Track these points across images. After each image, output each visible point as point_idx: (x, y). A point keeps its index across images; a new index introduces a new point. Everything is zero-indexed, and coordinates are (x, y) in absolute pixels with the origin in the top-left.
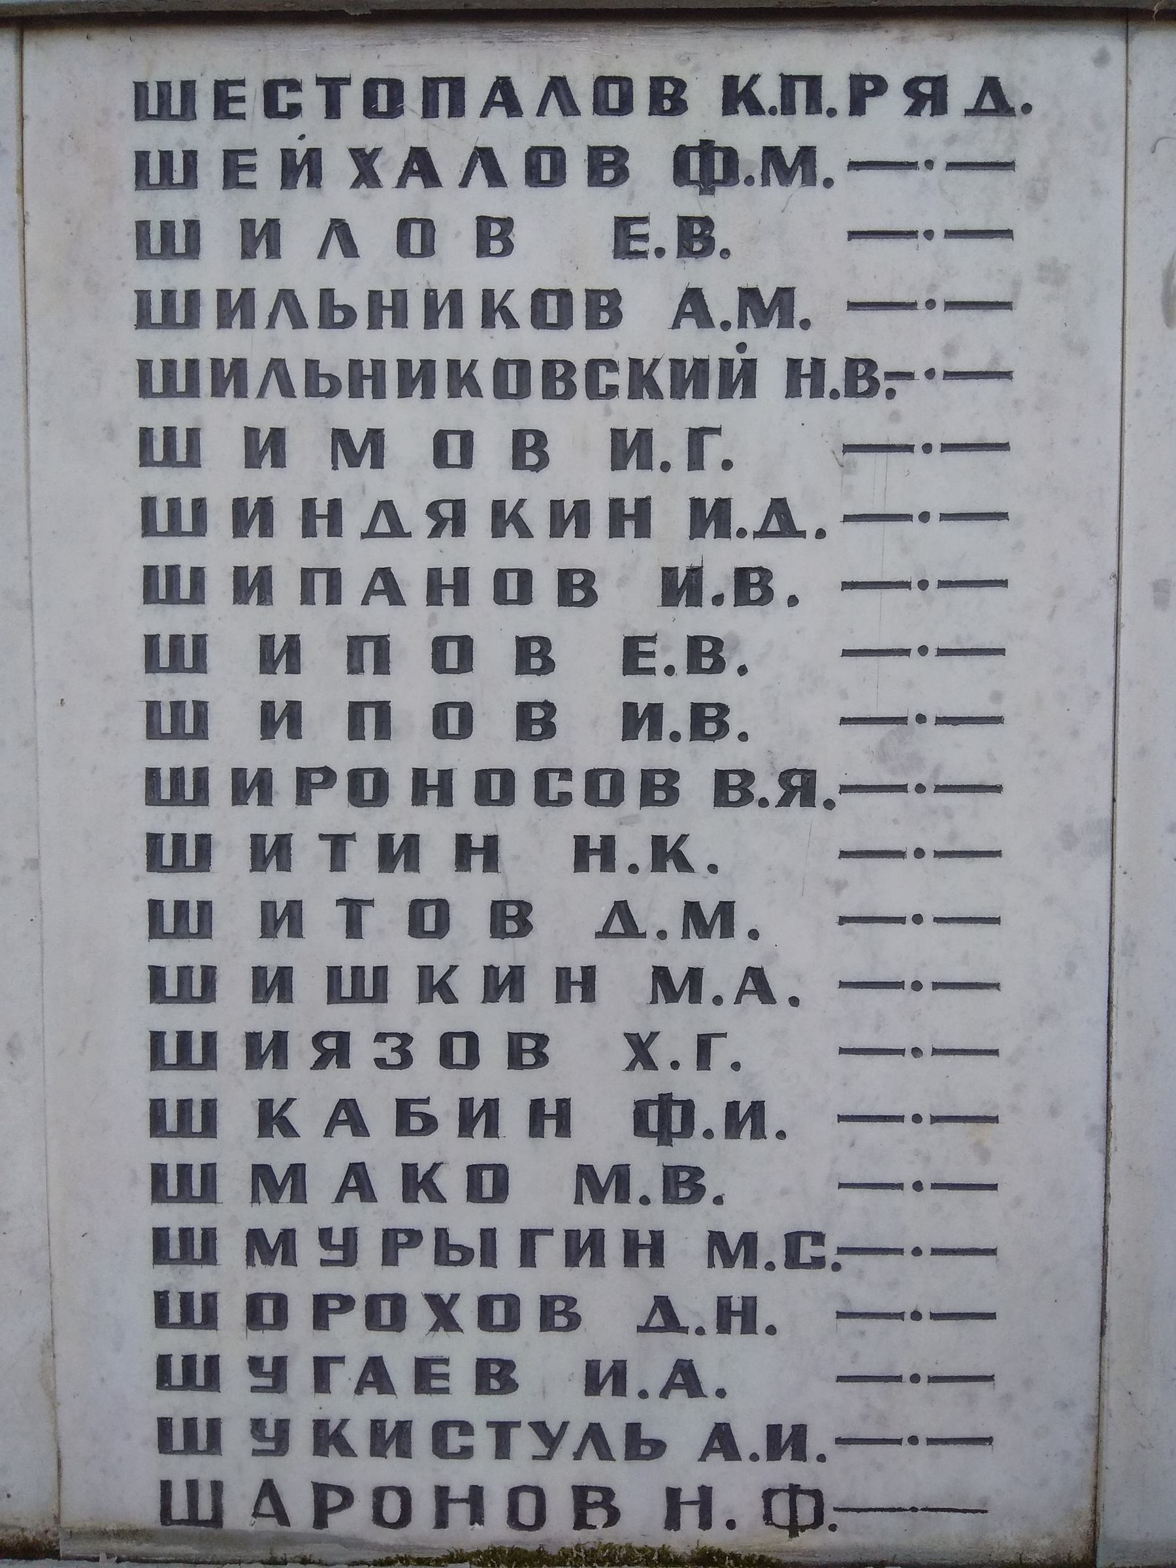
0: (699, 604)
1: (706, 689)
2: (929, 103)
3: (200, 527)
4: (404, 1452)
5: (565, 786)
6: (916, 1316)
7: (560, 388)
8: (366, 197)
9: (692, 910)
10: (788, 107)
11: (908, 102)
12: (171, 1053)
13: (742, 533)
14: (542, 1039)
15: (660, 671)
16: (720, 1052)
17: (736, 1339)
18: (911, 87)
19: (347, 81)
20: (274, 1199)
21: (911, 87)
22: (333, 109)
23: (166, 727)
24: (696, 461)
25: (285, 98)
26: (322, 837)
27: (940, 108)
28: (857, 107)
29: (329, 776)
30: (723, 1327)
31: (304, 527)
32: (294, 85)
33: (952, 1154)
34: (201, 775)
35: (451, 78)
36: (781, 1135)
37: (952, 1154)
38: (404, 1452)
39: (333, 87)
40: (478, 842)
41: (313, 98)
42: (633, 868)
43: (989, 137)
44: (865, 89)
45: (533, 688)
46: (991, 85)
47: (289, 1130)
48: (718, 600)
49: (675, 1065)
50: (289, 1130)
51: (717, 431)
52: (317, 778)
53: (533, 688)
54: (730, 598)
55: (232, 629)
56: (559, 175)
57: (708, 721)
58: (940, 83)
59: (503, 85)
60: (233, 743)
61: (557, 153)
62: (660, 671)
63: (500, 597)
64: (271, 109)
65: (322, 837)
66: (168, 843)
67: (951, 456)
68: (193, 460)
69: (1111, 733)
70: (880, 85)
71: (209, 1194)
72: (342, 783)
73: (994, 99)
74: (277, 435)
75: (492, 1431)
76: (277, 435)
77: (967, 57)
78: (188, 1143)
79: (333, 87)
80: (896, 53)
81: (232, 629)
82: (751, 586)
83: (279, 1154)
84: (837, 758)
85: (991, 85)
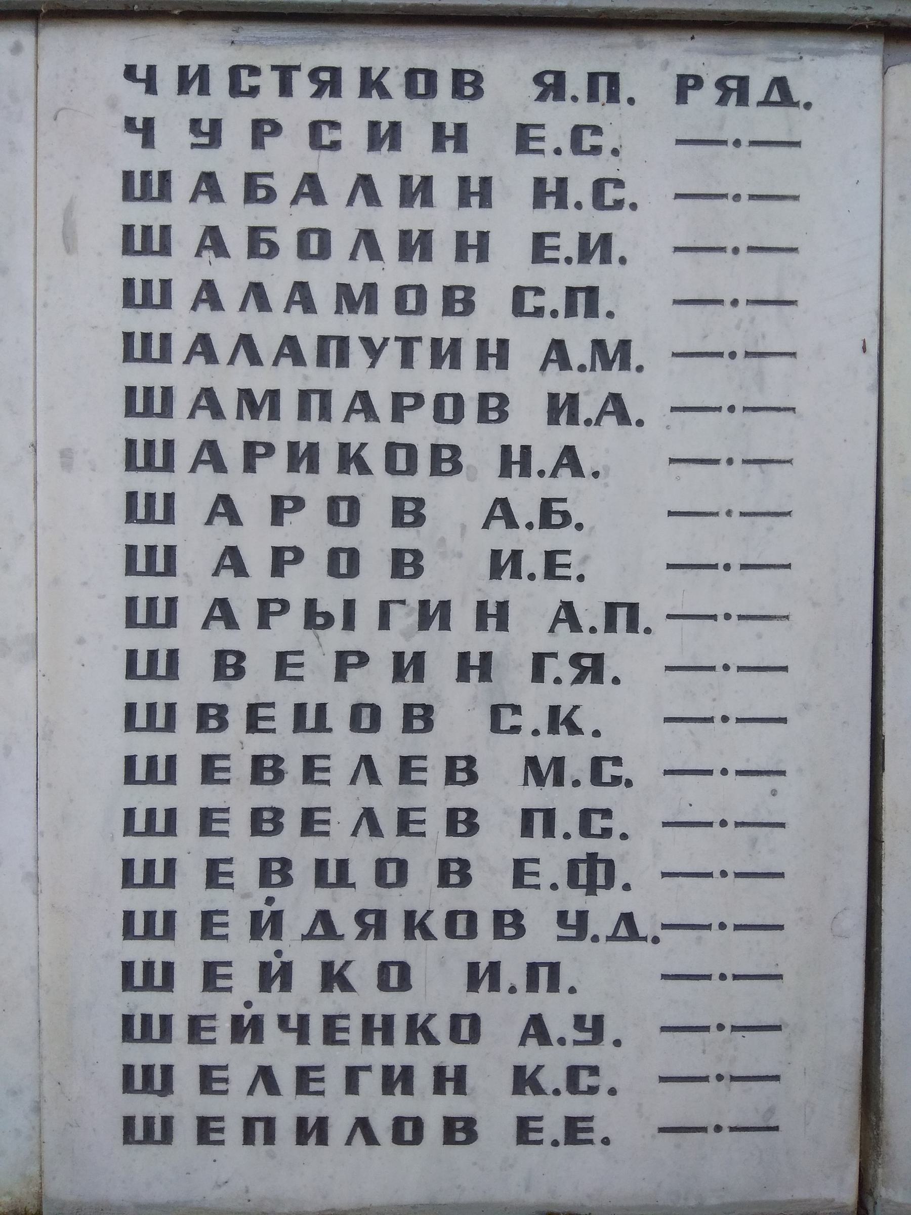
0: (529, 475)
3: (170, 725)
9: (599, 345)
12: (141, 772)
13: (595, 939)
15: (562, 260)
18: (721, 83)
19: (298, 68)
21: (721, 83)
22: (286, 89)
23: (138, 246)
25: (246, 82)
26: (353, 885)
27: (743, 100)
29: (270, 449)
32: (254, 71)
34: (166, 1020)
39: (285, 73)
41: (269, 82)
42: (575, 99)
43: (773, 122)
45: (406, 538)
46: (780, 83)
48: (530, 526)
52: (260, 450)
53: (406, 538)
55: (194, 490)
58: (743, 81)
60: (186, 998)
62: (562, 260)
64: (235, 90)
65: (353, 885)
66: (141, 501)
68: (169, 518)
70: (699, 82)
71: (167, 1087)
73: (782, 92)
75: (276, 74)
78: (146, 312)
79: (285, 73)
81: (194, 490)
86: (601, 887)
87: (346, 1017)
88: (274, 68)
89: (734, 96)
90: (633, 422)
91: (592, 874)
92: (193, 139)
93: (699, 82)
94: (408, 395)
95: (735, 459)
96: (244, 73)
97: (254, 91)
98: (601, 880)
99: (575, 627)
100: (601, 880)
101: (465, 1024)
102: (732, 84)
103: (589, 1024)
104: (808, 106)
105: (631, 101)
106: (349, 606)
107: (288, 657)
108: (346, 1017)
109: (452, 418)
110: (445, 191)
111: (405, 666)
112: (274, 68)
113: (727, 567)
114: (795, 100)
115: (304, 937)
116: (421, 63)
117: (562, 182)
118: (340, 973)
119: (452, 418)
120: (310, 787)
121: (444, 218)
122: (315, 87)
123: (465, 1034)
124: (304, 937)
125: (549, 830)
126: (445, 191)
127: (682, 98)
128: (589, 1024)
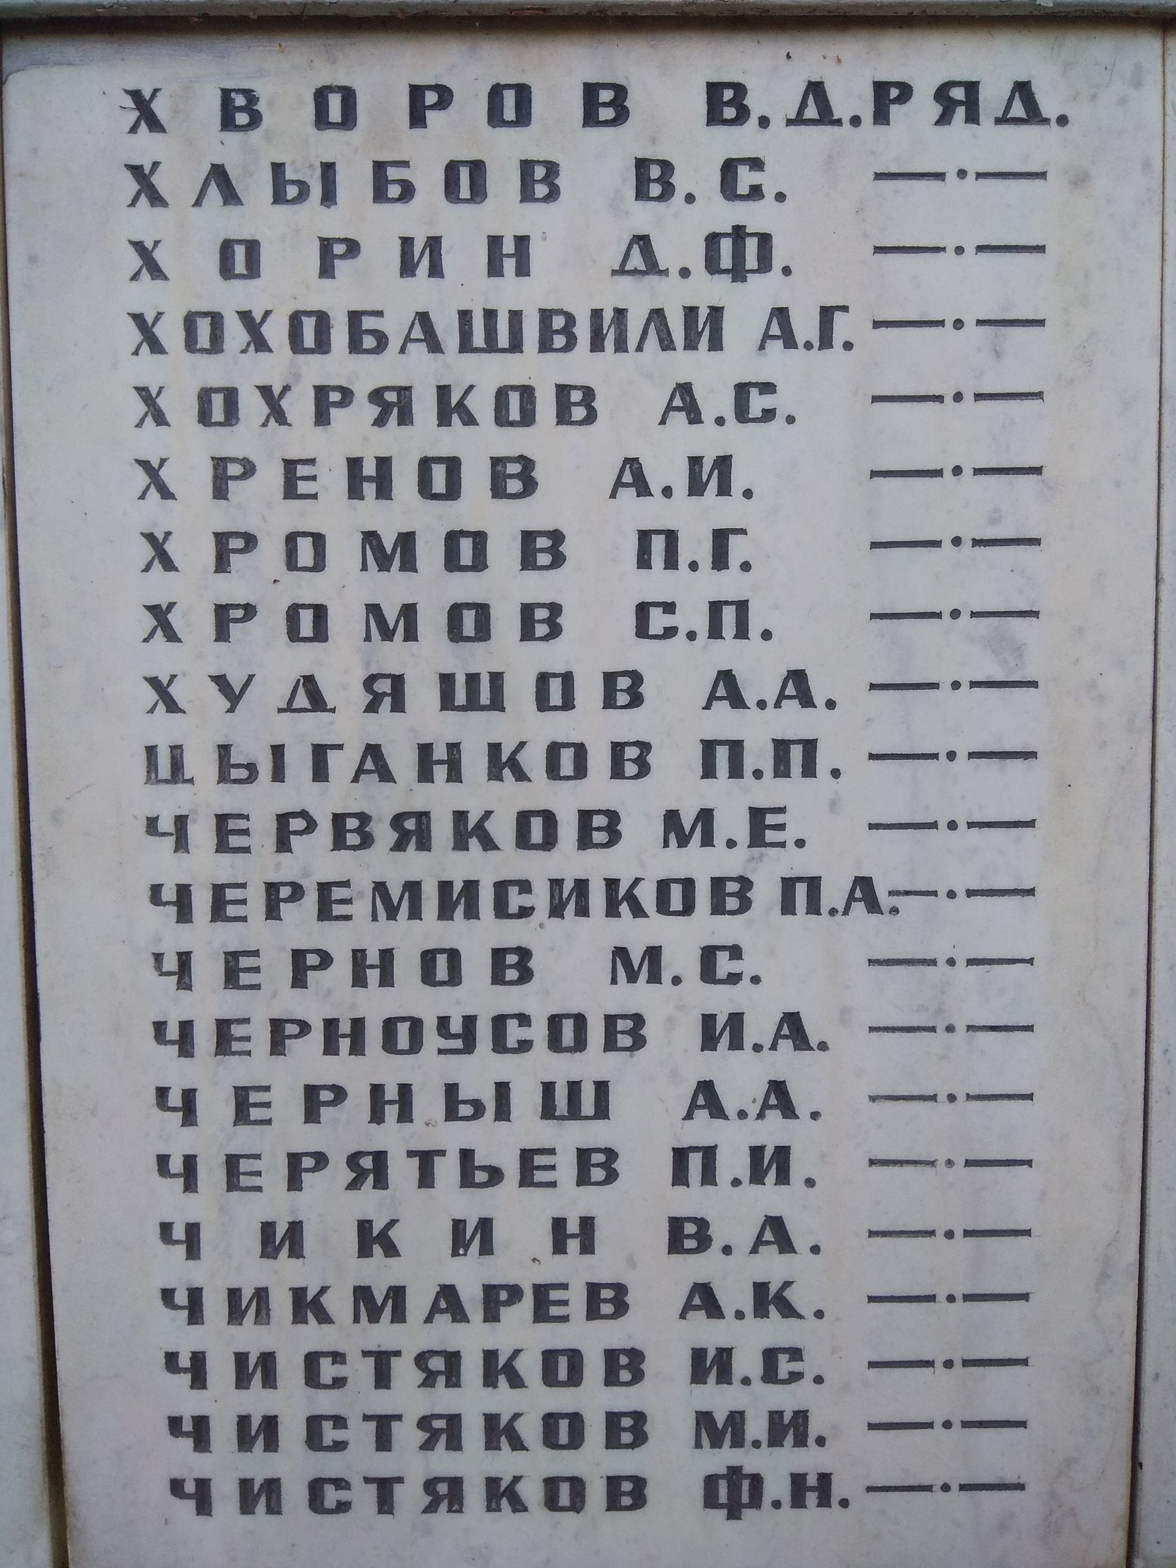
1: (786, 1399)
5: (526, 900)
7: (541, 190)
8: (271, 104)
10: (757, 1176)
11: (428, 1499)
13: (757, 1048)
14: (557, 537)
16: (738, 549)
17: (812, 1511)
24: (720, 560)
27: (973, 117)
28: (881, 116)
30: (798, 1501)
31: (218, 1044)
35: (380, 1416)
44: (888, 97)
46: (1023, 89)
51: (743, 532)
54: (768, 771)
56: (578, 1503)
57: (773, 1164)
58: (972, 88)
61: (549, 819)
67: (928, 1292)
69: (1157, 843)
72: (311, 898)
77: (993, 62)
80: (928, 60)
82: (795, 757)
86: (752, 271)
87: (564, 1286)
89: (960, 112)
90: (801, 344)
91: (738, 254)
93: (906, 91)
94: (233, 460)
98: (751, 262)
99: (695, 417)
100: (751, 262)
101: (218, 401)
102: (958, 94)
104: (1063, 120)
106: (502, 1089)
108: (564, 1286)
109: (339, 120)
110: (504, 551)
111: (455, 897)
113: (958, 324)
114: (1044, 116)
116: (342, 78)
118: (480, 826)
119: (339, 120)
120: (233, 993)
121: (505, 586)
122: (428, 1499)
123: (218, 414)
125: (671, 562)
126: (504, 551)
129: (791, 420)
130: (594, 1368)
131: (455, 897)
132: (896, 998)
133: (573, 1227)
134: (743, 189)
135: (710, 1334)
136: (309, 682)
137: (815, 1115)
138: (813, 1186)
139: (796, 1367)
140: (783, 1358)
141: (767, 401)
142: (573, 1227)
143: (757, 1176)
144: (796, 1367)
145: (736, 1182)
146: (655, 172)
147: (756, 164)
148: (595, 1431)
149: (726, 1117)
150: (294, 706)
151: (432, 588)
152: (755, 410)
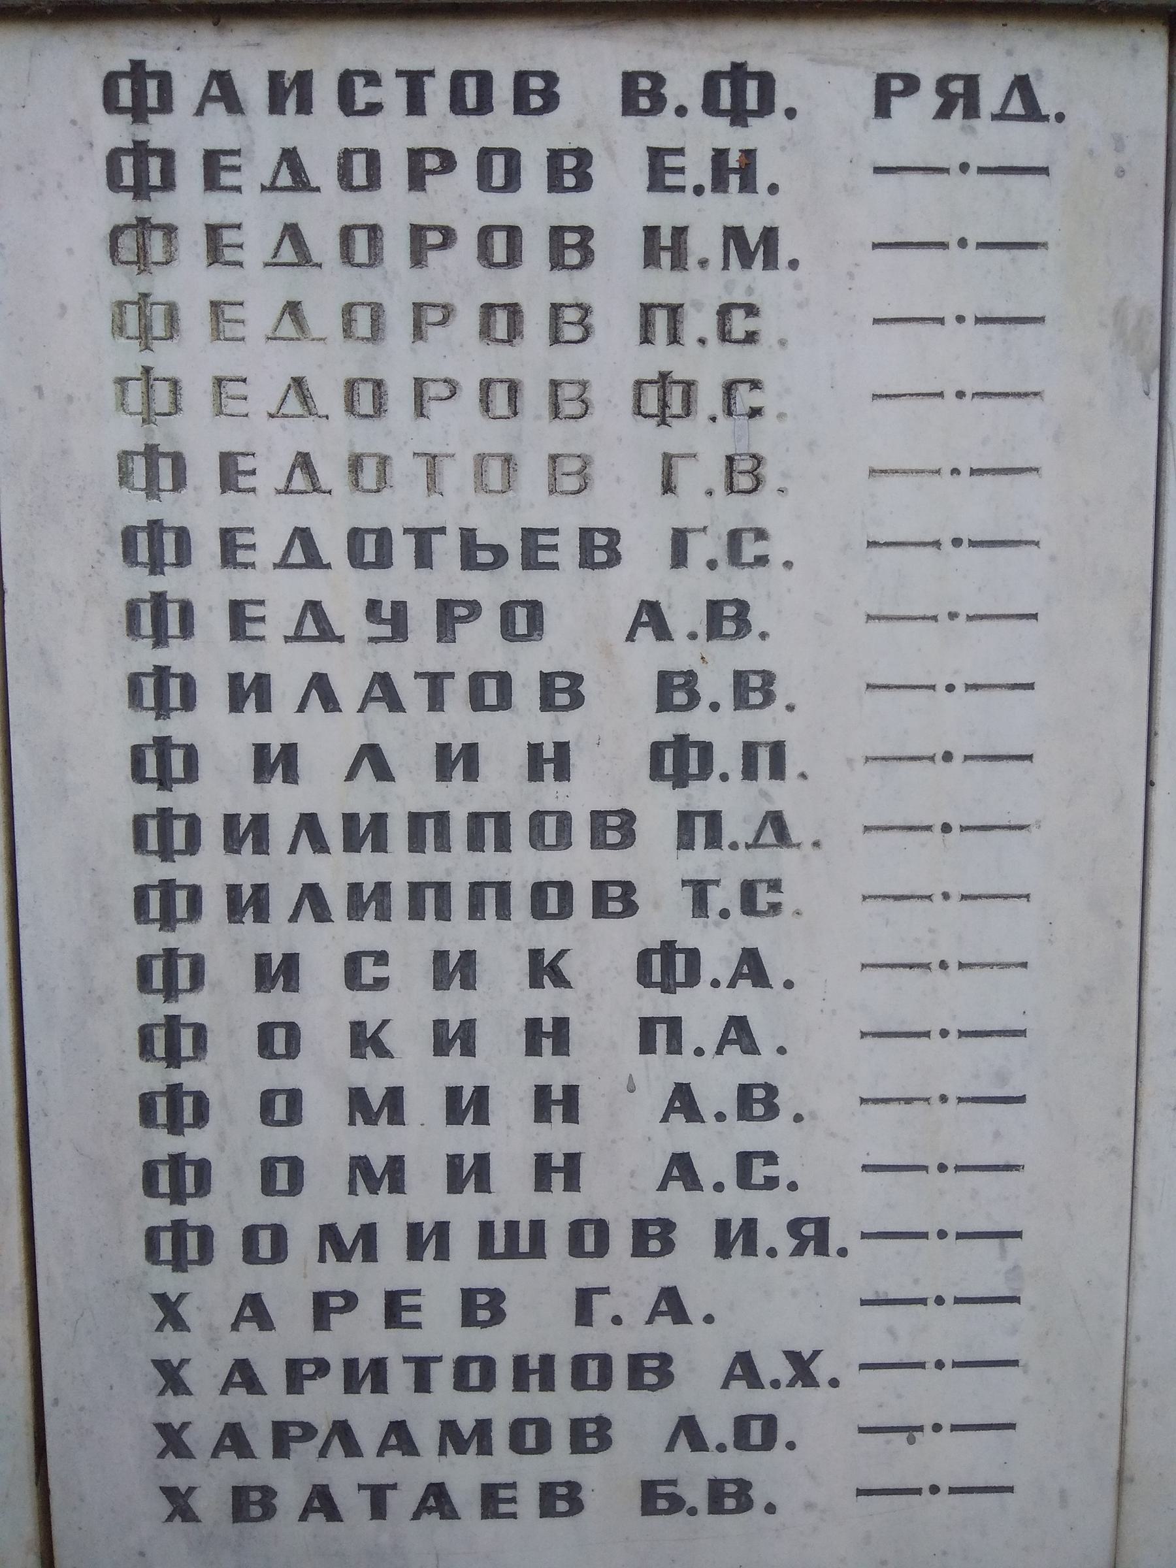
2: (812, 1243)
4: (380, 846)
6: (940, 1300)
10: (719, 184)
20: (373, 1189)
25: (363, 95)
26: (361, 1487)
27: (971, 111)
32: (372, 79)
33: (982, 1269)
36: (789, 984)
37: (982, 1269)
38: (380, 846)
39: (415, 81)
40: (558, 1161)
43: (1022, 142)
46: (1022, 84)
47: (383, 1052)
49: (703, 263)
50: (383, 1052)
58: (971, 82)
59: (222, 78)
63: (602, 1227)
65: (361, 1487)
69: (1139, 1150)
70: (911, 84)
74: (468, 957)
75: (402, 83)
76: (468, 957)
77: (991, 54)
79: (415, 81)
83: (375, 1076)
84: (852, 1205)
85: (1022, 84)
88: (399, 74)
92: (678, 1491)
95: (955, 755)
96: (359, 82)
97: (373, 109)
102: (957, 87)
103: (386, 613)
104: (1060, 117)
105: (791, 113)
107: (331, 1299)
111: (465, 1174)
112: (399, 74)
115: (276, 566)
117: (680, 233)
124: (276, 566)
127: (882, 109)
128: (386, 613)
129: (793, 1186)
130: (534, 172)
131: (465, 1174)
132: (877, 1335)
133: (557, 1112)
134: (738, 334)
135: (666, 211)
136: (313, 607)
137: (788, 564)
138: (790, 568)
139: (771, 1171)
140: (757, 1163)
141: (760, 548)
142: (557, 1112)
143: (719, 184)
144: (771, 1171)
145: (715, 983)
146: (645, 84)
147: (755, 384)
148: (536, 247)
149: (763, 1387)
150: (290, 561)
151: (534, 284)
152: (758, 1177)
